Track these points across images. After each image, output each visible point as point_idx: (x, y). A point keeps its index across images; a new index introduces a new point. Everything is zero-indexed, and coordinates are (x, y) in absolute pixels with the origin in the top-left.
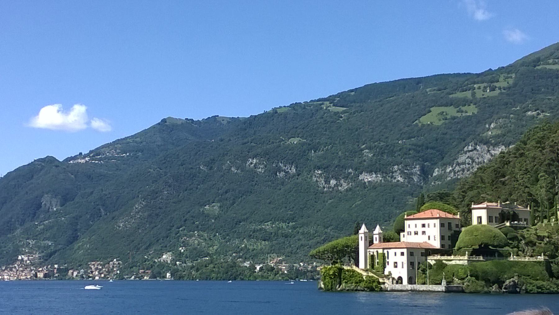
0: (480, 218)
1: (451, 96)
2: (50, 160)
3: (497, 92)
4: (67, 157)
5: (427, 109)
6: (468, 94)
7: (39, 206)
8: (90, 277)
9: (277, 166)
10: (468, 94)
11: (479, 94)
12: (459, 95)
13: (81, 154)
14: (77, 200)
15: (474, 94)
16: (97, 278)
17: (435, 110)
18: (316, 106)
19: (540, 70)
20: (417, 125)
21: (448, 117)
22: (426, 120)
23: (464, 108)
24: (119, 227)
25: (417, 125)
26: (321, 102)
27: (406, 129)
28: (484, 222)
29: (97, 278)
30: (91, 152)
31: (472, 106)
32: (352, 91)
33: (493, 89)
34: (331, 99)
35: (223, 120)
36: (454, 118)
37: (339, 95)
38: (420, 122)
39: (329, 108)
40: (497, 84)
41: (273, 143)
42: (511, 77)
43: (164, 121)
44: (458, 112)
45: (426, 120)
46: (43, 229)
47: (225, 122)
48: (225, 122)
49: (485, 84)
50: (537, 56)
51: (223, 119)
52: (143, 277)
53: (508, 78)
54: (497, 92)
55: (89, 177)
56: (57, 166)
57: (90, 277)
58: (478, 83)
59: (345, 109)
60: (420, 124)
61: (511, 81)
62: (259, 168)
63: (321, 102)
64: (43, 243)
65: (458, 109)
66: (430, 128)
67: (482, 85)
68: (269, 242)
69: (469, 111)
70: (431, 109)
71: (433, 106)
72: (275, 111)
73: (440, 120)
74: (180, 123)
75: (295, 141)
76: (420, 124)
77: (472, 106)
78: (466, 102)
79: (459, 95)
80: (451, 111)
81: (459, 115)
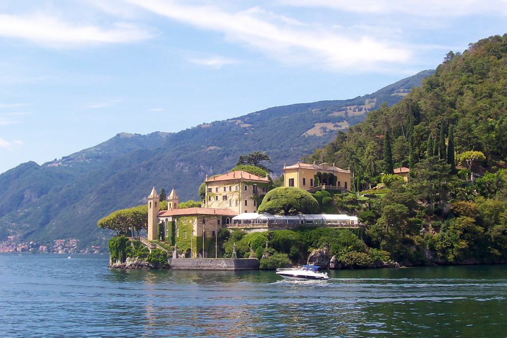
0: (292, 182)
1: (329, 115)
2: (31, 165)
3: (364, 111)
4: (424, 70)
5: (312, 125)
6: (342, 114)
7: (22, 198)
8: (55, 251)
9: (198, 167)
10: (342, 114)
11: (351, 113)
12: (336, 114)
13: (56, 160)
14: (49, 193)
15: (346, 113)
16: (60, 252)
17: (318, 126)
18: (232, 123)
19: (394, 96)
20: (304, 136)
21: (327, 130)
22: (310, 132)
23: (338, 124)
24: (78, 213)
25: (304, 136)
26: (235, 121)
27: (296, 139)
28: (296, 185)
29: (60, 252)
30: (63, 158)
31: (345, 122)
32: (258, 112)
33: (360, 110)
34: (242, 118)
35: (163, 135)
36: (331, 131)
37: (249, 115)
38: (306, 134)
39: (241, 125)
40: (363, 107)
41: (195, 150)
42: (373, 101)
43: (118, 135)
44: (334, 126)
45: (310, 132)
46: (24, 215)
47: (164, 137)
48: (164, 137)
49: (355, 106)
50: (392, 87)
51: (163, 133)
52: (94, 251)
53: (371, 102)
54: (364, 111)
55: (61, 177)
56: (36, 168)
57: (55, 251)
58: (349, 106)
59: (251, 125)
60: (306, 136)
61: (373, 104)
62: (185, 169)
63: (235, 121)
64: (24, 225)
65: (335, 124)
66: (313, 138)
67: (352, 107)
68: (194, 238)
69: (342, 126)
70: (315, 124)
71: (316, 123)
72: (199, 126)
73: (321, 133)
74: (130, 136)
75: (212, 148)
76: (306, 136)
77: (345, 122)
78: (341, 119)
79: (336, 114)
80: (330, 126)
81: (336, 129)
